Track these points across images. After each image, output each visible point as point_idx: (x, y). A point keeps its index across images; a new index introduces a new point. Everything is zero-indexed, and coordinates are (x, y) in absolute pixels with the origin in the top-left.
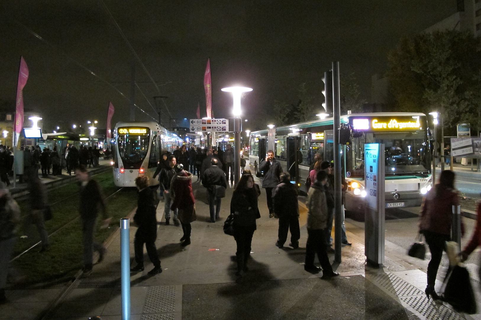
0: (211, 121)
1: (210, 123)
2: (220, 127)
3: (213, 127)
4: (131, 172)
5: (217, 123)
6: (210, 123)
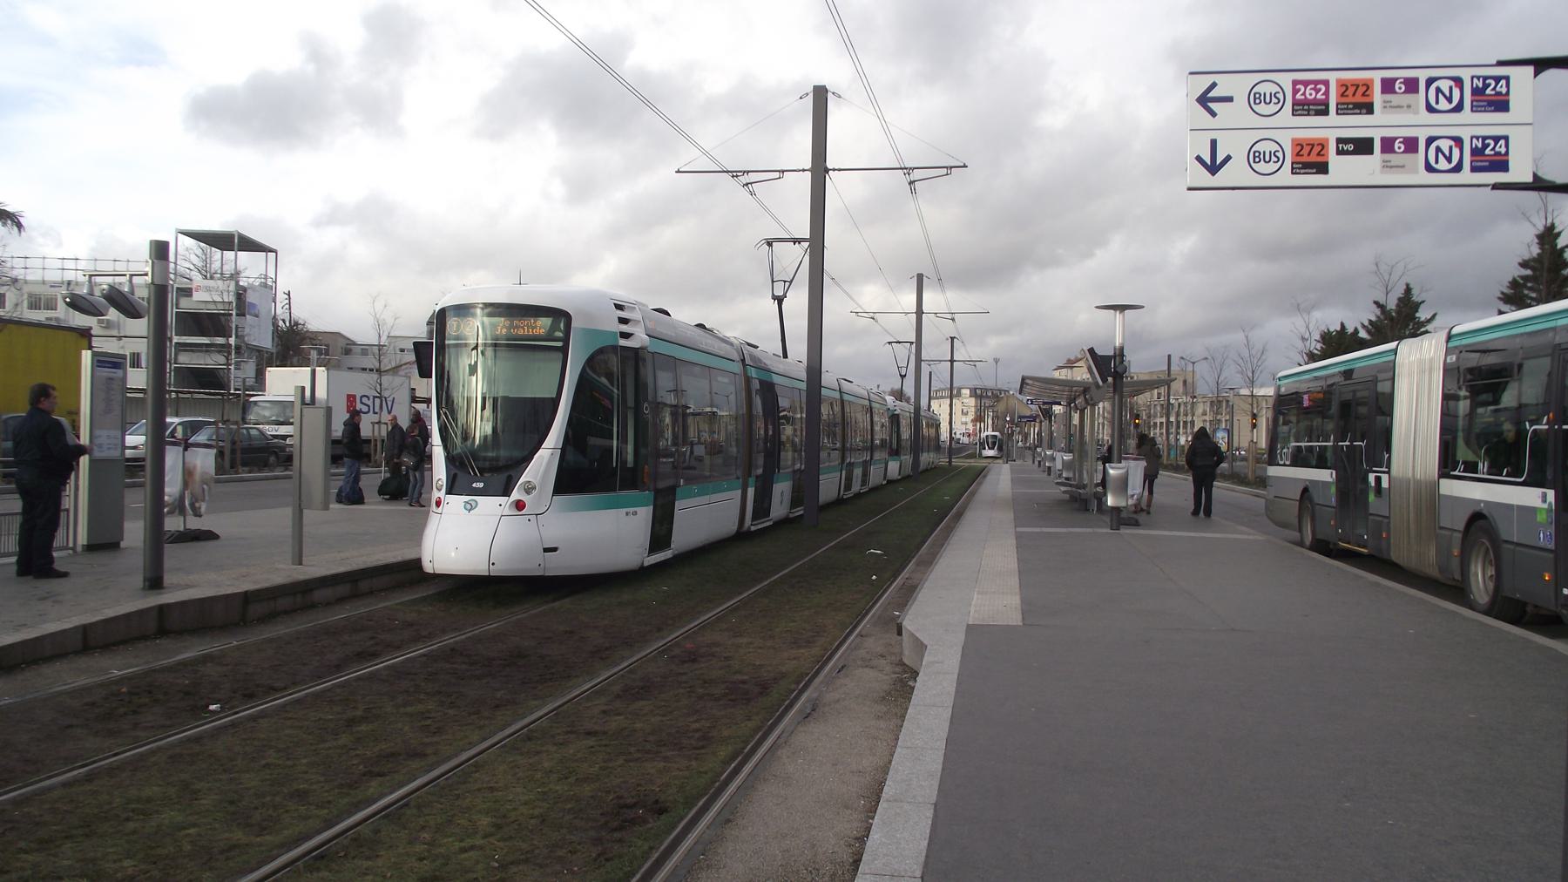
0: (1377, 87)
1: (1368, 108)
2: (1458, 141)
3: (1388, 145)
4: (470, 507)
5: (1430, 109)
6: (1368, 108)
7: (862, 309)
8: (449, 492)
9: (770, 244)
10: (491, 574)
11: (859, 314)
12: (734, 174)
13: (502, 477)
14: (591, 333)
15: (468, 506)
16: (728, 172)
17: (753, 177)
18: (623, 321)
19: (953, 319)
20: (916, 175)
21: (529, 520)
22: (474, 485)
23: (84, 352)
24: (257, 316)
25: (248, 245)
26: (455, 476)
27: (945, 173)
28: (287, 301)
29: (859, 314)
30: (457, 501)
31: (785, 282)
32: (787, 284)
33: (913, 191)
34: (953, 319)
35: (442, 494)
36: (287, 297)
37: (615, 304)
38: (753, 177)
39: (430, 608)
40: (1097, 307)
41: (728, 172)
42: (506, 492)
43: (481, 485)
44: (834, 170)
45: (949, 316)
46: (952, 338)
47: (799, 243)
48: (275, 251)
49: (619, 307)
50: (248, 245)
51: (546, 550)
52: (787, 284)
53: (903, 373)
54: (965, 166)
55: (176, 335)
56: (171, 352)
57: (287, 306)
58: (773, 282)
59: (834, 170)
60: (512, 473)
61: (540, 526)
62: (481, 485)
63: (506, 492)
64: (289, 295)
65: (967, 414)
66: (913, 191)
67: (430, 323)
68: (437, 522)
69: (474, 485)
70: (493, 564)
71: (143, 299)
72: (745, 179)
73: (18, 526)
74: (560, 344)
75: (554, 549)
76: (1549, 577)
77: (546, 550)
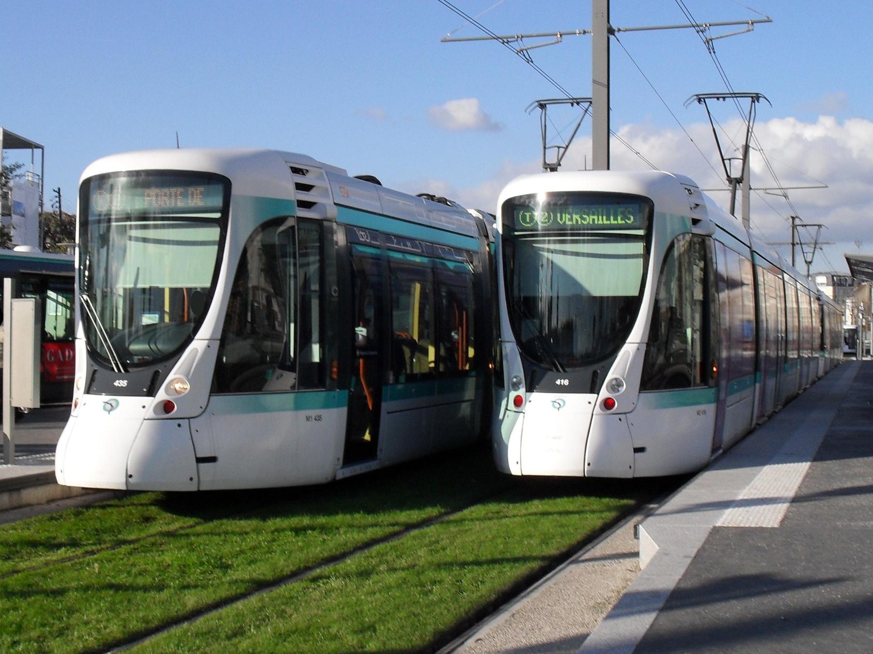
4: (111, 408)
8: (88, 391)
9: (542, 106)
12: (505, 41)
13: (148, 372)
14: (262, 202)
15: (109, 407)
16: (497, 38)
17: (527, 43)
18: (300, 187)
19: (786, 196)
20: (712, 33)
21: (620, 420)
23: (5, 279)
24: (23, 215)
25: (671, 246)
26: (95, 372)
27: (746, 29)
28: (57, 199)
30: (99, 400)
31: (559, 147)
32: (562, 150)
33: (711, 50)
34: (786, 196)
35: (522, 392)
36: (57, 194)
37: (291, 168)
38: (527, 43)
39: (759, 545)
41: (497, 38)
42: (151, 393)
43: (566, 382)
45: (779, 192)
46: (793, 218)
47: (578, 103)
48: (42, 148)
49: (295, 170)
50: (671, 246)
52: (562, 150)
53: (809, 260)
54: (769, 21)
57: (58, 204)
58: (545, 148)
60: (160, 368)
61: (193, 431)
62: (123, 383)
63: (594, 388)
64: (59, 193)
65: (165, 193)
66: (711, 50)
72: (517, 46)
74: (217, 215)
75: (213, 459)
76: (470, 367)
77: (200, 460)
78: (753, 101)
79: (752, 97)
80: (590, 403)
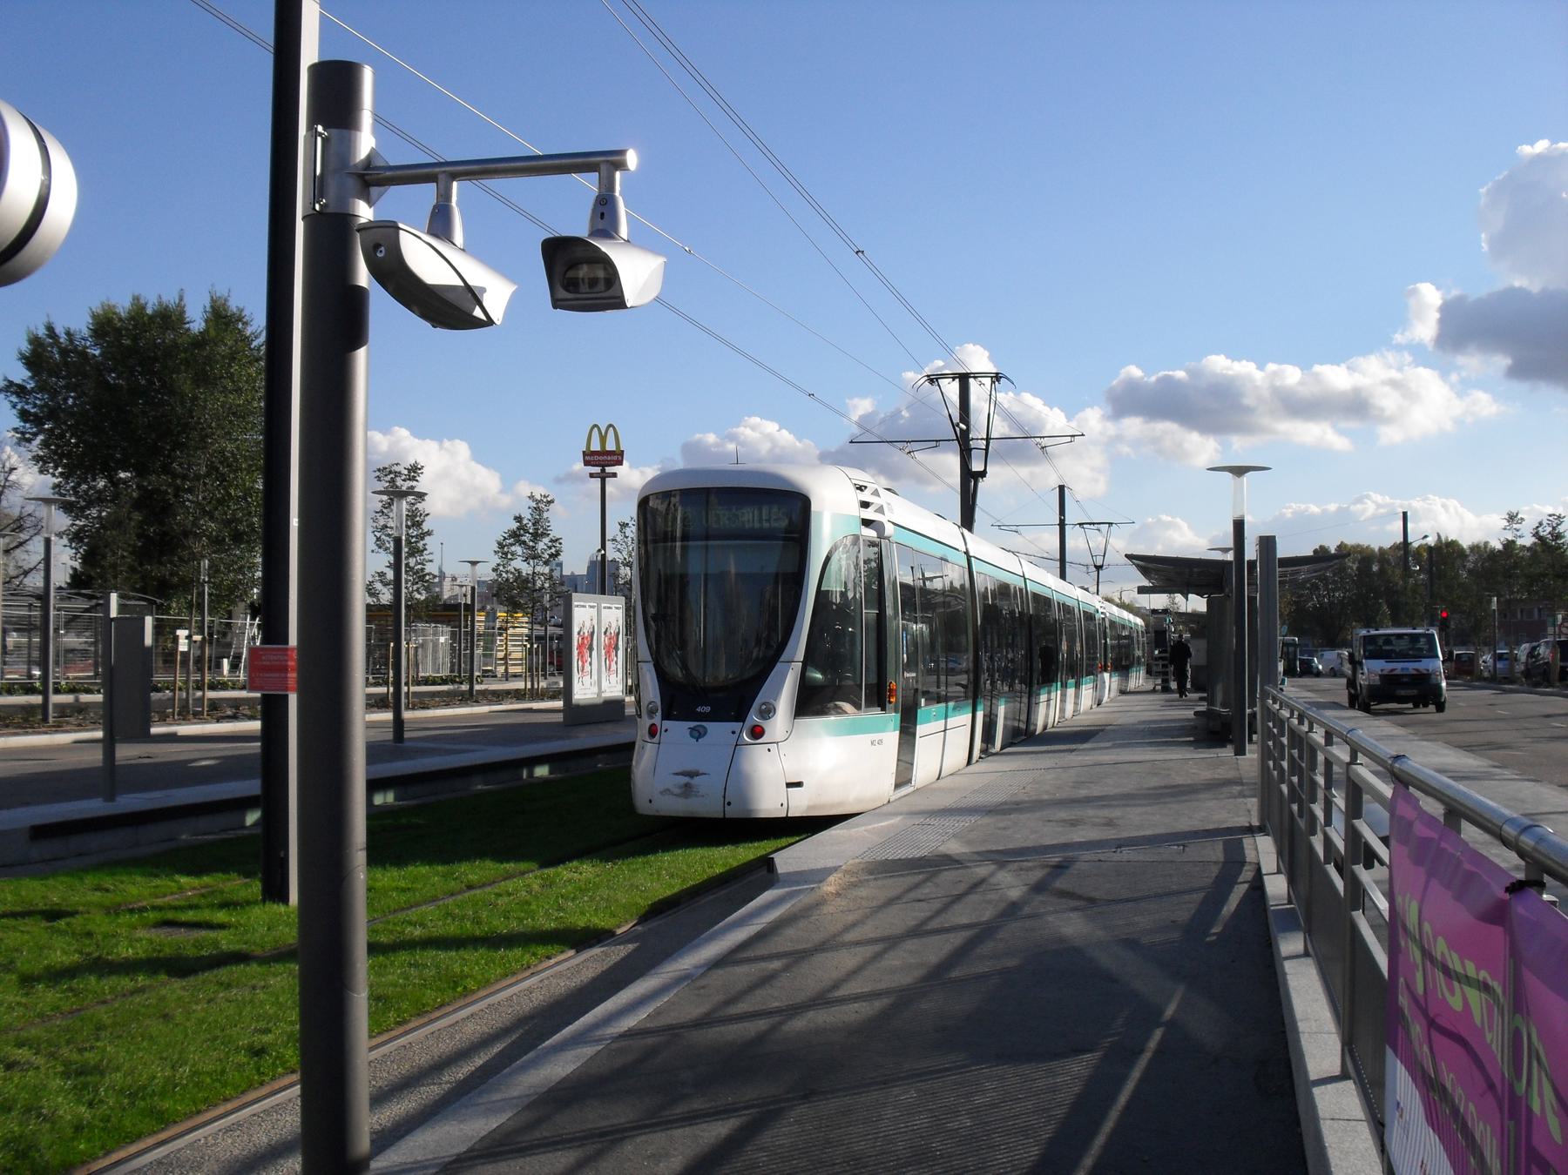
4: (698, 734)
7: (1089, 517)
8: (667, 716)
10: (727, 816)
11: (1002, 527)
15: (696, 734)
21: (769, 750)
22: (699, 709)
29: (1002, 527)
35: (657, 719)
40: (1270, 469)
43: (708, 709)
44: (953, 440)
51: (789, 785)
53: (1099, 563)
55: (1279, 567)
56: (476, 627)
59: (953, 440)
62: (708, 709)
67: (688, 582)
68: (1459, 724)
69: (699, 709)
70: (729, 804)
71: (1225, 550)
73: (1377, 722)
75: (799, 784)
77: (789, 785)
78: (993, 382)
79: (992, 377)
80: (734, 733)
